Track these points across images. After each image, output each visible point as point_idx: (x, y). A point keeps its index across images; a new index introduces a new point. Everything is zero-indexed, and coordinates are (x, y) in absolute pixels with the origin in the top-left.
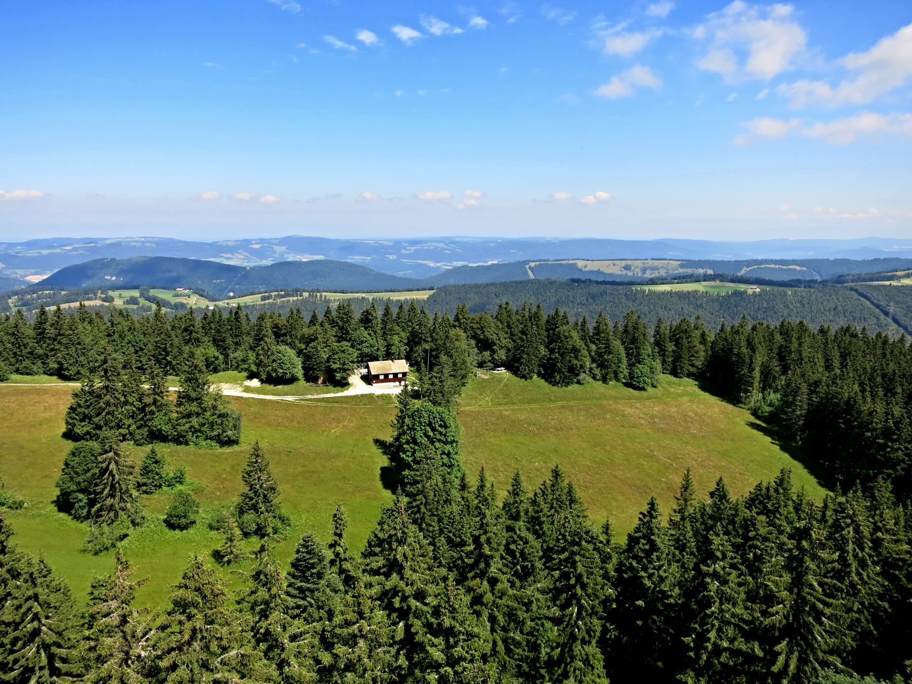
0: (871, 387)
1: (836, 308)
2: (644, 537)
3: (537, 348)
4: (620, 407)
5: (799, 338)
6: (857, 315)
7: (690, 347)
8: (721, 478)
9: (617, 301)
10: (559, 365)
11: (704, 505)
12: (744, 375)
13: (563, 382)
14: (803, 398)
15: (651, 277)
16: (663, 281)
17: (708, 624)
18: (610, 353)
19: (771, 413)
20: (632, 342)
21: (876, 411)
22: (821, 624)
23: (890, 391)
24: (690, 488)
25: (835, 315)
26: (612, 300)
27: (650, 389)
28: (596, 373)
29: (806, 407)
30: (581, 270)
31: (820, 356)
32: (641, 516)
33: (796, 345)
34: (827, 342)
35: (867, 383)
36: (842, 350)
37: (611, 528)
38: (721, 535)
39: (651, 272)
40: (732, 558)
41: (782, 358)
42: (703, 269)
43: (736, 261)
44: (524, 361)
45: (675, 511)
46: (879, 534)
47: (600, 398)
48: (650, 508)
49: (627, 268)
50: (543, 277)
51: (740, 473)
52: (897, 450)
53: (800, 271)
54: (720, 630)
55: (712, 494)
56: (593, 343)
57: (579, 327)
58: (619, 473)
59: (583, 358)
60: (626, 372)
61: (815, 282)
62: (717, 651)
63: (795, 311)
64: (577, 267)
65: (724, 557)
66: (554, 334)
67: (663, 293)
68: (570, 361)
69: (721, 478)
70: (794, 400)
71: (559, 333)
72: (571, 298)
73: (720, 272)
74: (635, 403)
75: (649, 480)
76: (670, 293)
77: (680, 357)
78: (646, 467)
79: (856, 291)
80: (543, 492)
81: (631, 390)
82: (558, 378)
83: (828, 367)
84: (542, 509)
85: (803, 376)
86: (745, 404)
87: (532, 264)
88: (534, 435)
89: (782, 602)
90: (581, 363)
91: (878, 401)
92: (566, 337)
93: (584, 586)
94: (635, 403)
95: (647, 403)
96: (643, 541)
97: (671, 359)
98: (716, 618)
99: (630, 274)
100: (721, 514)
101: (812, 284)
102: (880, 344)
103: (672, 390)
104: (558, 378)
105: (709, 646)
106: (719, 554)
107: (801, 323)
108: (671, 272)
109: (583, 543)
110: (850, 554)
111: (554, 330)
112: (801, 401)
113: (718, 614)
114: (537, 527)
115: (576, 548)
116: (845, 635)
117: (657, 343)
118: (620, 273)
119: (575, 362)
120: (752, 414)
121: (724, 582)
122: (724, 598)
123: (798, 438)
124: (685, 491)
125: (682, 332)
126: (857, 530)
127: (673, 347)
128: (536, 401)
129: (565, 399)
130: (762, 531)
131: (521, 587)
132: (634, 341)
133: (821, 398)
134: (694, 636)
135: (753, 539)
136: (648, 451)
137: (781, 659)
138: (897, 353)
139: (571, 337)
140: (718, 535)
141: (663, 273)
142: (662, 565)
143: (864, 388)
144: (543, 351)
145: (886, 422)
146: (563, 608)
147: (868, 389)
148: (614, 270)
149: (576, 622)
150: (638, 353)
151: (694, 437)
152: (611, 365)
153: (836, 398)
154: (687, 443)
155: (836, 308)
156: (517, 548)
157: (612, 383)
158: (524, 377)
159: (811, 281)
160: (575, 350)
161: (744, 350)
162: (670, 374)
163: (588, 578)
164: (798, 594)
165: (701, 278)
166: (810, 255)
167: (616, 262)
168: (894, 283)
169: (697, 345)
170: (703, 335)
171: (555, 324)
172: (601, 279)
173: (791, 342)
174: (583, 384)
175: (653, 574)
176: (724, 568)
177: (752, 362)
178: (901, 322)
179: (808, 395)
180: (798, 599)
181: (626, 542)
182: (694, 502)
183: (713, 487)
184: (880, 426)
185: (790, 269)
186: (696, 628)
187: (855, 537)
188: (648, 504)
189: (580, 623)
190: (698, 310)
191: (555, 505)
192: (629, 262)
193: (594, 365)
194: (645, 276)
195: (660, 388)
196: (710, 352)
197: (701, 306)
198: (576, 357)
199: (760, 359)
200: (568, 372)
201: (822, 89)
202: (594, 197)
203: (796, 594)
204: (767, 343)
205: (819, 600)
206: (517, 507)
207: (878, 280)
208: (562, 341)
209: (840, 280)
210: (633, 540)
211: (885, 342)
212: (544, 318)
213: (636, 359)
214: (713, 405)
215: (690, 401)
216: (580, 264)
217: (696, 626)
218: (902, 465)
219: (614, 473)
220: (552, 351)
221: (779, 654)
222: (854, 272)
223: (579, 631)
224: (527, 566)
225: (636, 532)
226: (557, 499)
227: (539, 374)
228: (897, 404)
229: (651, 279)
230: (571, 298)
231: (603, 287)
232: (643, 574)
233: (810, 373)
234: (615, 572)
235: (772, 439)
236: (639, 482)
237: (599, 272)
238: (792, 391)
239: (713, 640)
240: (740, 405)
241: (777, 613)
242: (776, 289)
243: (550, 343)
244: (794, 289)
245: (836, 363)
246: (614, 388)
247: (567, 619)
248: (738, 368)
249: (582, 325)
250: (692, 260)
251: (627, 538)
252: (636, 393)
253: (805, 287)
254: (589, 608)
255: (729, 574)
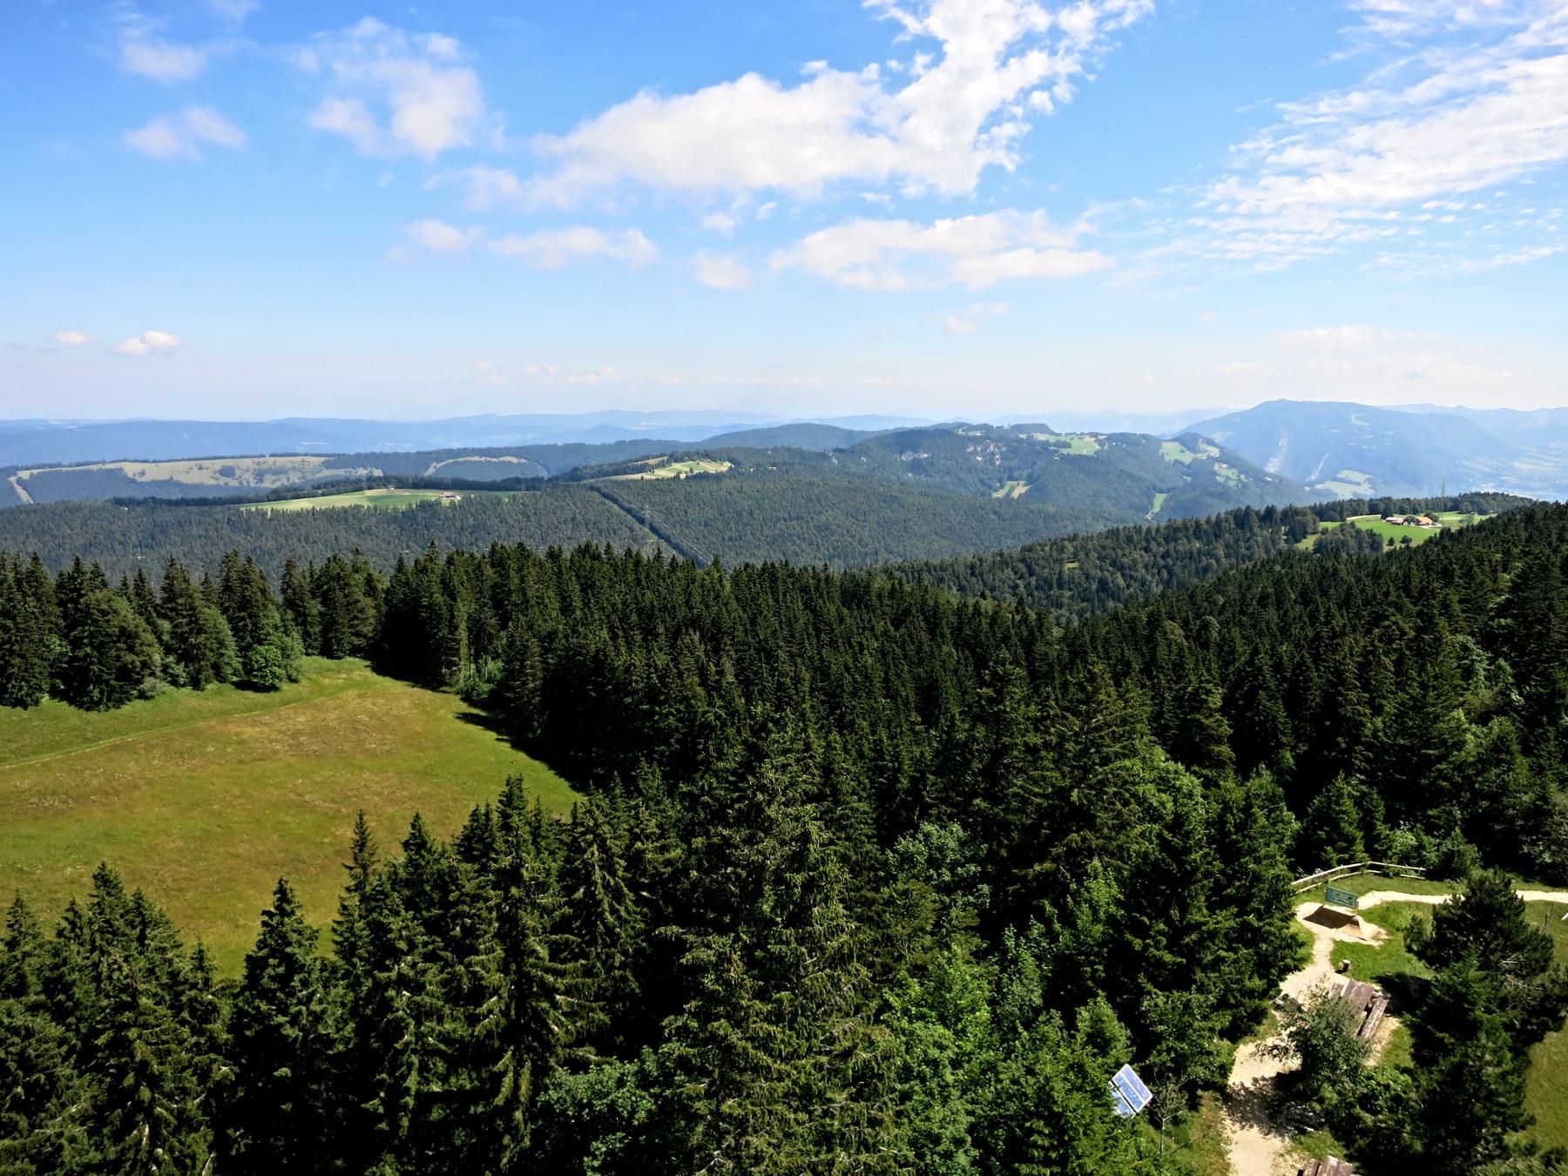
0: (624, 631)
1: (573, 519)
2: (272, 954)
3: (41, 640)
4: (233, 728)
5: (520, 570)
6: (604, 526)
7: (349, 604)
8: (19, 903)
9: (212, 533)
10: (95, 668)
11: (394, 866)
12: (443, 638)
13: (109, 700)
14: (534, 662)
15: (274, 487)
16: (296, 493)
17: (402, 1065)
18: (200, 631)
19: (492, 692)
20: (242, 608)
21: (634, 664)
22: (555, 1005)
23: (649, 633)
24: (369, 844)
25: (573, 530)
26: (203, 532)
27: (286, 687)
28: (177, 672)
29: (540, 674)
30: (133, 481)
31: (551, 594)
32: (266, 918)
33: (516, 581)
34: (560, 571)
35: (619, 626)
36: (583, 581)
37: (208, 955)
38: (403, 912)
39: (273, 477)
40: (425, 944)
41: (498, 604)
42: (365, 468)
43: (419, 453)
44: (15, 670)
45: (348, 890)
46: (638, 844)
47: (191, 718)
48: (279, 900)
49: (227, 472)
50: (50, 498)
51: (454, 799)
52: (667, 716)
53: (519, 464)
54: (423, 1069)
55: (406, 845)
56: (165, 617)
57: (131, 590)
58: (242, 849)
59: (145, 648)
60: (237, 663)
61: (540, 480)
62: (426, 1100)
63: (517, 529)
64: (125, 477)
65: (412, 946)
66: (76, 609)
67: (299, 514)
68: (118, 658)
69: (19, 903)
70: (523, 666)
71: (88, 606)
72: (118, 536)
73: (392, 472)
74: (259, 716)
75: (302, 846)
76: (313, 513)
77: (334, 622)
78: (293, 825)
79: (598, 490)
80: (72, 923)
81: (250, 694)
82: (96, 694)
83: (566, 610)
84: (66, 958)
85: (531, 628)
86: (451, 686)
87: (25, 475)
88: (55, 815)
89: (496, 992)
90: (142, 658)
91: (636, 650)
92: (104, 613)
93: (155, 1082)
94: (259, 716)
95: (283, 712)
96: (271, 961)
97: (318, 629)
98: (414, 1052)
99: (233, 483)
100: (422, 875)
101: (537, 485)
102: (631, 566)
103: (327, 681)
104: (96, 694)
105: (410, 1101)
106: (402, 945)
107: (521, 545)
108: (309, 476)
109: (143, 1000)
110: (599, 886)
111: (76, 602)
112: (532, 667)
113: (416, 1043)
114: (61, 997)
115: (127, 1016)
116: (593, 1010)
117: (290, 603)
118: (214, 482)
119: (129, 657)
120: (463, 700)
121: (418, 988)
122: (420, 1013)
123: (535, 724)
124: (361, 851)
125: (333, 578)
126: (604, 848)
127: (319, 607)
128: (55, 746)
129: (116, 732)
130: (469, 887)
131: (32, 1127)
132: (244, 604)
133: (559, 657)
134: (382, 1094)
135: (458, 902)
136: (292, 796)
137: (508, 1081)
138: (653, 576)
139: (115, 612)
140: (397, 914)
141: (296, 479)
142: (313, 993)
143: (614, 633)
144: (57, 645)
145: (649, 678)
146: (118, 1137)
147: (621, 633)
148: (200, 477)
149: (151, 1152)
150: (255, 624)
151: (373, 754)
152: (204, 654)
153: (580, 654)
154: (361, 769)
155: (573, 519)
156: (7, 1053)
157: (212, 687)
158: (20, 703)
159: (535, 480)
160: (127, 636)
161: (439, 598)
162: (321, 654)
163: (161, 1064)
164: (519, 971)
165: (364, 485)
166: (530, 439)
167: (205, 463)
168: (647, 476)
169: (361, 598)
170: (369, 581)
171: (78, 590)
172: (176, 495)
173: (508, 578)
174: (152, 697)
175: (299, 1013)
176: (414, 966)
177: (453, 616)
178: (662, 531)
179: (541, 655)
180: (519, 979)
181: (245, 972)
182: (379, 867)
183: (406, 832)
184: (641, 685)
185: (503, 462)
186: (383, 1080)
187: (602, 860)
188: (275, 893)
189: (160, 1150)
190: (364, 540)
191: (98, 942)
192: (228, 463)
193: (171, 659)
194: (262, 485)
195: (304, 682)
196: (384, 609)
197: (368, 532)
198: (131, 649)
199: (464, 609)
200: (115, 679)
201: (506, 181)
202: (142, 341)
203: (515, 973)
204: (474, 582)
205: (547, 970)
206: (18, 968)
207: (625, 473)
208: (97, 621)
209: (574, 476)
210: (255, 965)
211: (638, 563)
212: (52, 579)
213: (252, 637)
214: (400, 696)
215: (360, 696)
216: (131, 469)
217: (384, 1075)
218: (677, 736)
219: (233, 850)
220: (76, 644)
221: (504, 1074)
222: (593, 463)
223: (159, 1168)
224: (38, 1080)
225: (260, 949)
226: (101, 930)
227: (54, 693)
228: (660, 650)
229: (275, 491)
230: (118, 536)
231: (182, 512)
232: (281, 1019)
233: (540, 622)
234: (228, 1032)
235: (498, 733)
236: (282, 854)
237: (170, 483)
238: (518, 653)
239: (414, 1088)
240: (444, 688)
241: (490, 1011)
242: (485, 494)
243: (72, 625)
244: (512, 493)
245: (578, 603)
246: (217, 696)
247: (131, 1155)
248: (432, 628)
249: (137, 586)
250: (344, 455)
251: (245, 964)
252: (260, 697)
253: (527, 490)
254: (171, 1118)
255: (424, 971)
